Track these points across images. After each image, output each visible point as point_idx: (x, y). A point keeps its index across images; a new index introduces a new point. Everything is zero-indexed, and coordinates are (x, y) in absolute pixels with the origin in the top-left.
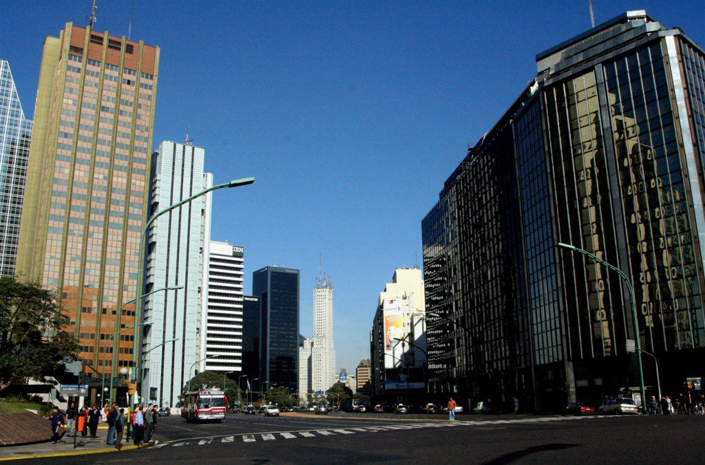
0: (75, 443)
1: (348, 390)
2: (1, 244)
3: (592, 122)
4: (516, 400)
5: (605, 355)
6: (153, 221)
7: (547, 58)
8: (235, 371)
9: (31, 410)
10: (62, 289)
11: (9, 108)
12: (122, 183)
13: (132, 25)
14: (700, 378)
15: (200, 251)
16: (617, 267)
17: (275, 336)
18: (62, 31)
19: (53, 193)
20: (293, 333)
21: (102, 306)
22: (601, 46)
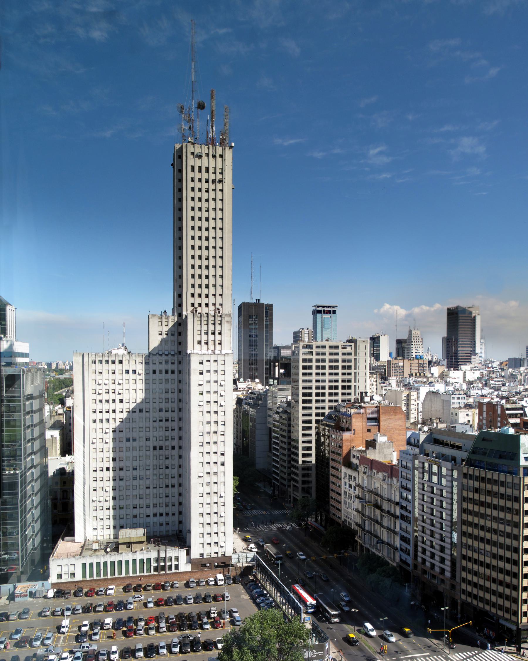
0: (194, 144)
1: (199, 641)
2: (22, 658)
3: (408, 485)
4: (259, 485)
5: (301, 459)
6: (401, 475)
7: (317, 335)
8: (234, 475)
9: (298, 140)
10: (29, 371)
11: (453, 360)
12: (214, 324)
13: (304, 587)
14: (314, 462)
15: (125, 345)
16: (31, 619)
17: (321, 418)
18: (501, 621)
19: (216, 584)
20: (401, 371)
21: (138, 643)
22: (186, 151)
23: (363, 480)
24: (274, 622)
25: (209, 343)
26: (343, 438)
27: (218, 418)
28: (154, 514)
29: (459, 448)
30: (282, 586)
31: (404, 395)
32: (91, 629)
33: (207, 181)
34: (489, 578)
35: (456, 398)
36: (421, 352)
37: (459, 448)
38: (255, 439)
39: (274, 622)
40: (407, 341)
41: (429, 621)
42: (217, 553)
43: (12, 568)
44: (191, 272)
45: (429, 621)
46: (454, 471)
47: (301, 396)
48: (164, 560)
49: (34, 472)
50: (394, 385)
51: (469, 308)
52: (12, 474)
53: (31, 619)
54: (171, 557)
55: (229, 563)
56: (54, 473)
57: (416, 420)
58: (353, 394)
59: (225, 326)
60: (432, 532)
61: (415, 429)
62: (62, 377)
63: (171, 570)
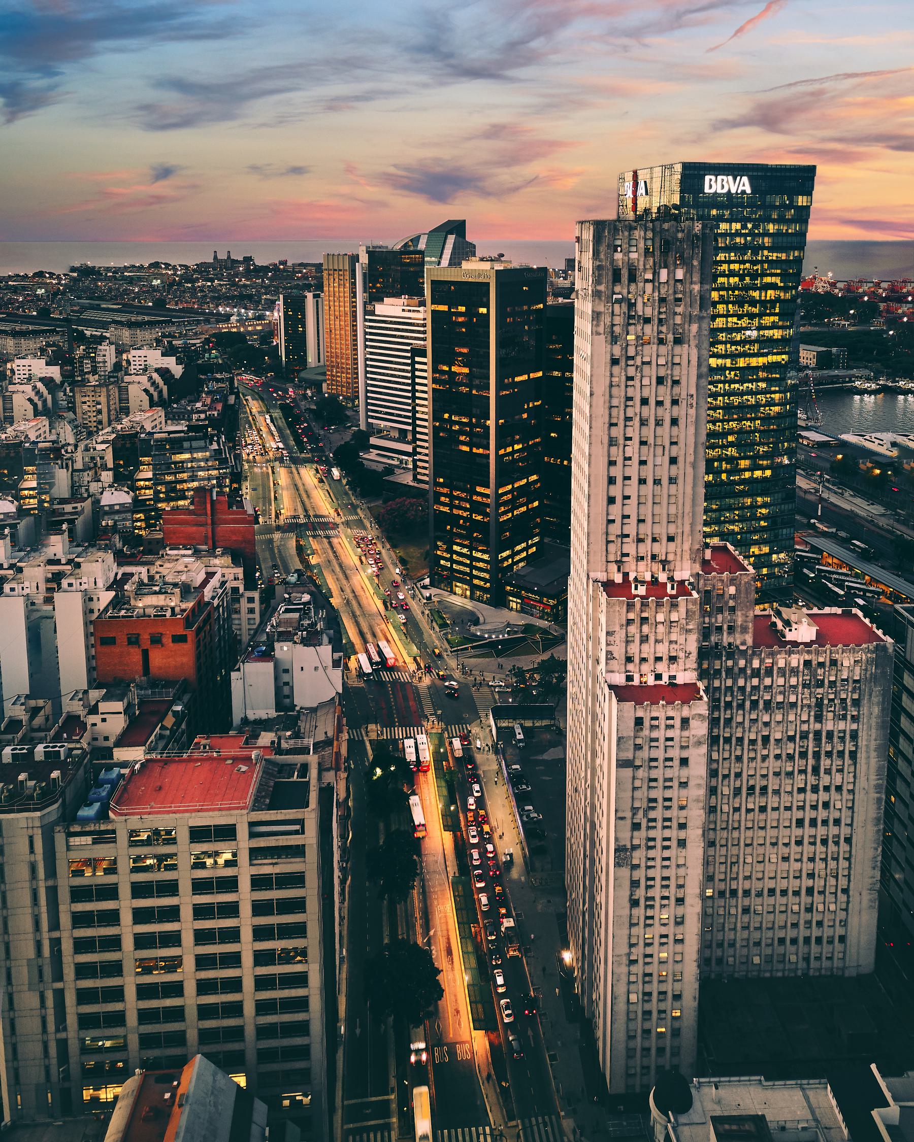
14: (749, 191)
23: (300, 493)
24: (632, 358)
25: (628, 883)
26: (810, 237)
27: (608, 471)
28: (670, 479)
29: (31, 838)
30: (343, 882)
31: (292, 543)
32: (259, 294)
33: (643, 422)
34: (380, 412)
35: (56, 934)
36: (457, 674)
37: (31, 838)
38: (333, 699)
39: (632, 358)
40: (828, 465)
41: (553, 435)
42: (501, 837)
43: (344, 899)
44: (678, 411)
45: (553, 435)
46: (621, 581)
47: (186, 985)
48: (720, 945)
49: (83, 875)
50: (518, 730)
51: (425, 86)
52: (735, 1131)
53: (905, 609)
54: (251, 865)
55: (11, 756)
56: (438, 971)
57: (177, 590)
58: (70, 999)
59: (865, 710)
60: (744, 928)
61: (809, 652)
62: (182, 1134)
63: (432, 303)
